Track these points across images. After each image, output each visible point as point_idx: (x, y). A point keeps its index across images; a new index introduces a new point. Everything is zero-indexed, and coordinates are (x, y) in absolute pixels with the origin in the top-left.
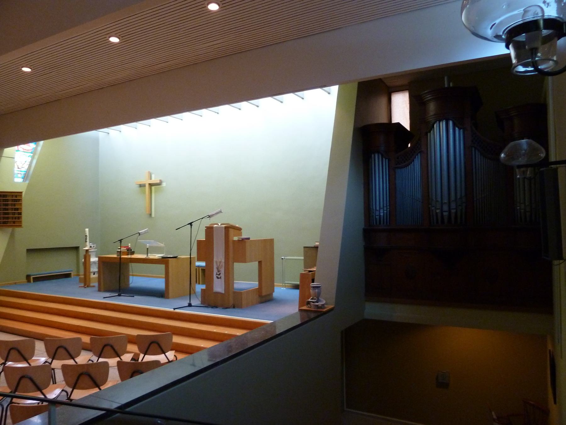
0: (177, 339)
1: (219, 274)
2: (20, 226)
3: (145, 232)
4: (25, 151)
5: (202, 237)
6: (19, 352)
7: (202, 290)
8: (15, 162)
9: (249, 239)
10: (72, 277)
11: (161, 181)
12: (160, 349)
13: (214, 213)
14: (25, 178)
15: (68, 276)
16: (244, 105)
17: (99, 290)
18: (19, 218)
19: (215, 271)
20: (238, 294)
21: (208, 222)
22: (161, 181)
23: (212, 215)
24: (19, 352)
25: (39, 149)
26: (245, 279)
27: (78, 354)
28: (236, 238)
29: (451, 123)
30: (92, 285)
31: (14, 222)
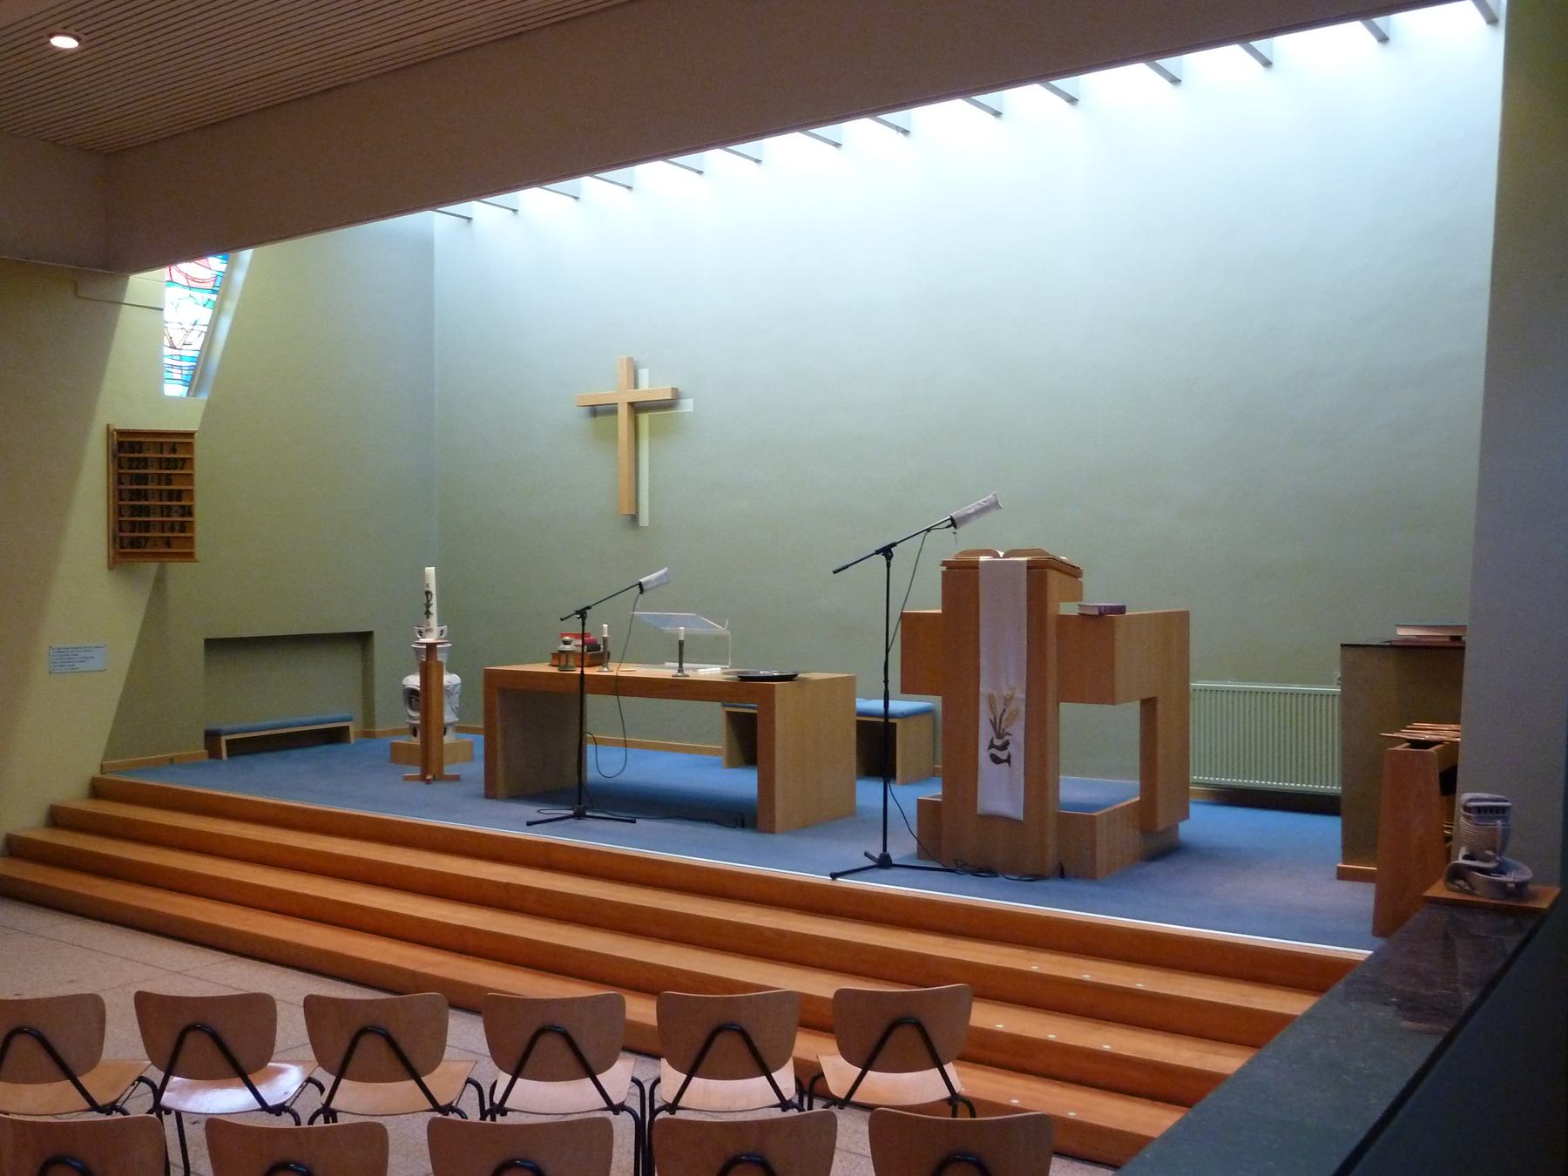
0: (989, 1018)
1: (1004, 747)
2: (189, 556)
3: (661, 583)
4: (192, 284)
5: (929, 602)
6: (392, 1044)
7: (921, 803)
8: (162, 325)
9: (1121, 610)
10: (353, 740)
11: (675, 391)
12: (925, 1051)
13: (971, 508)
14: (195, 382)
15: (336, 736)
16: (714, 158)
17: (491, 793)
18: (184, 527)
19: (985, 734)
20: (1079, 824)
21: (949, 547)
22: (675, 391)
23: (966, 518)
24: (392, 1044)
25: (240, 276)
26: (1097, 772)
27: (608, 1065)
28: (1069, 609)
30: (448, 770)
31: (168, 542)
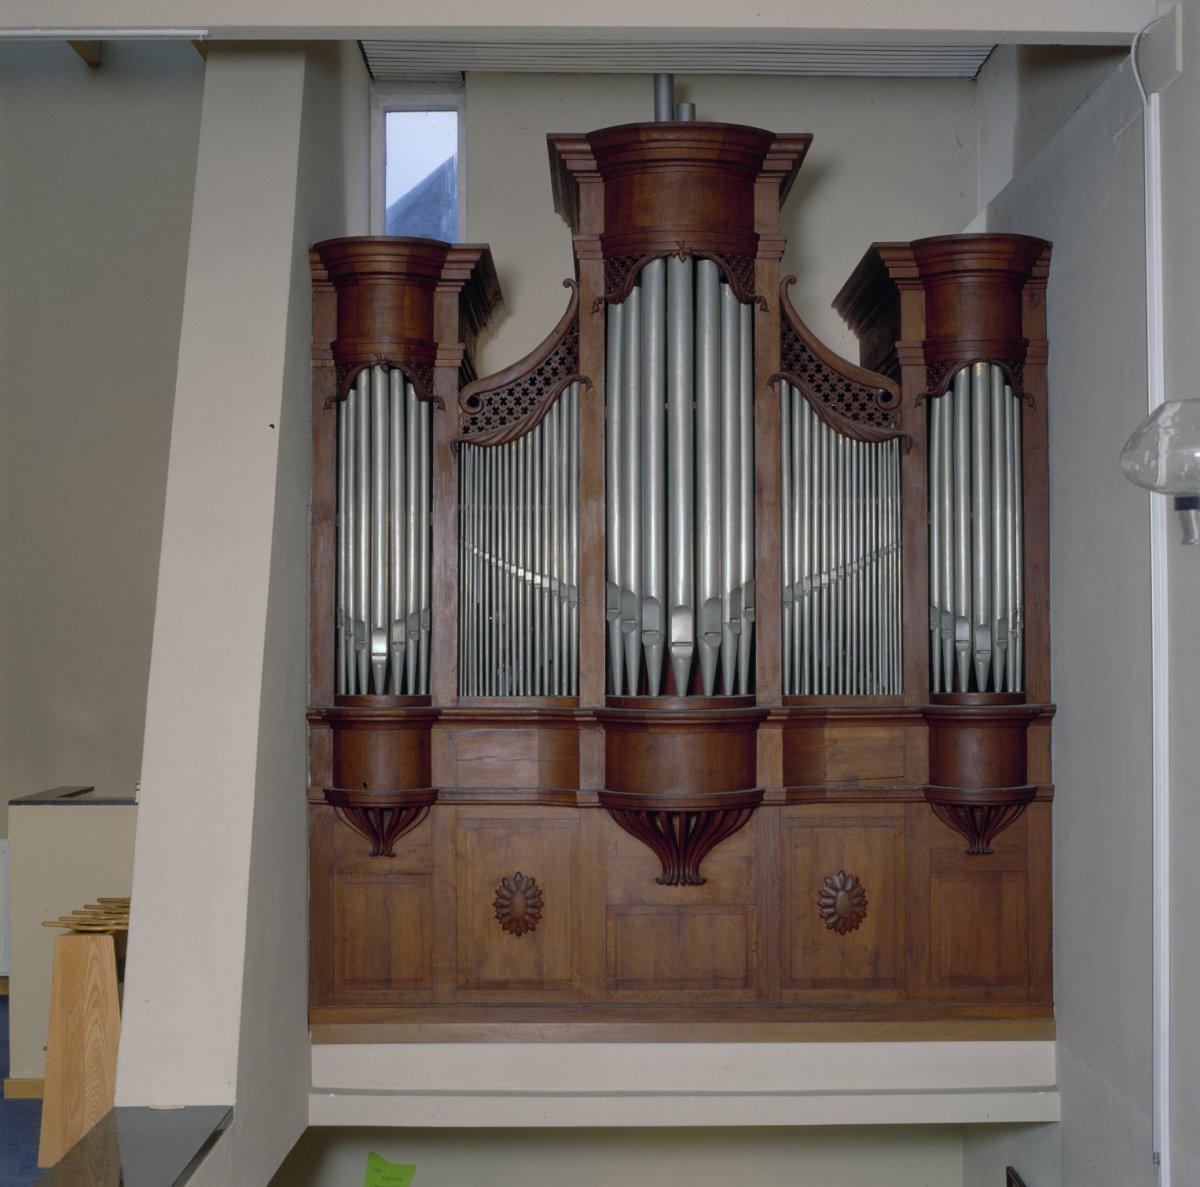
29: (707, 269)
